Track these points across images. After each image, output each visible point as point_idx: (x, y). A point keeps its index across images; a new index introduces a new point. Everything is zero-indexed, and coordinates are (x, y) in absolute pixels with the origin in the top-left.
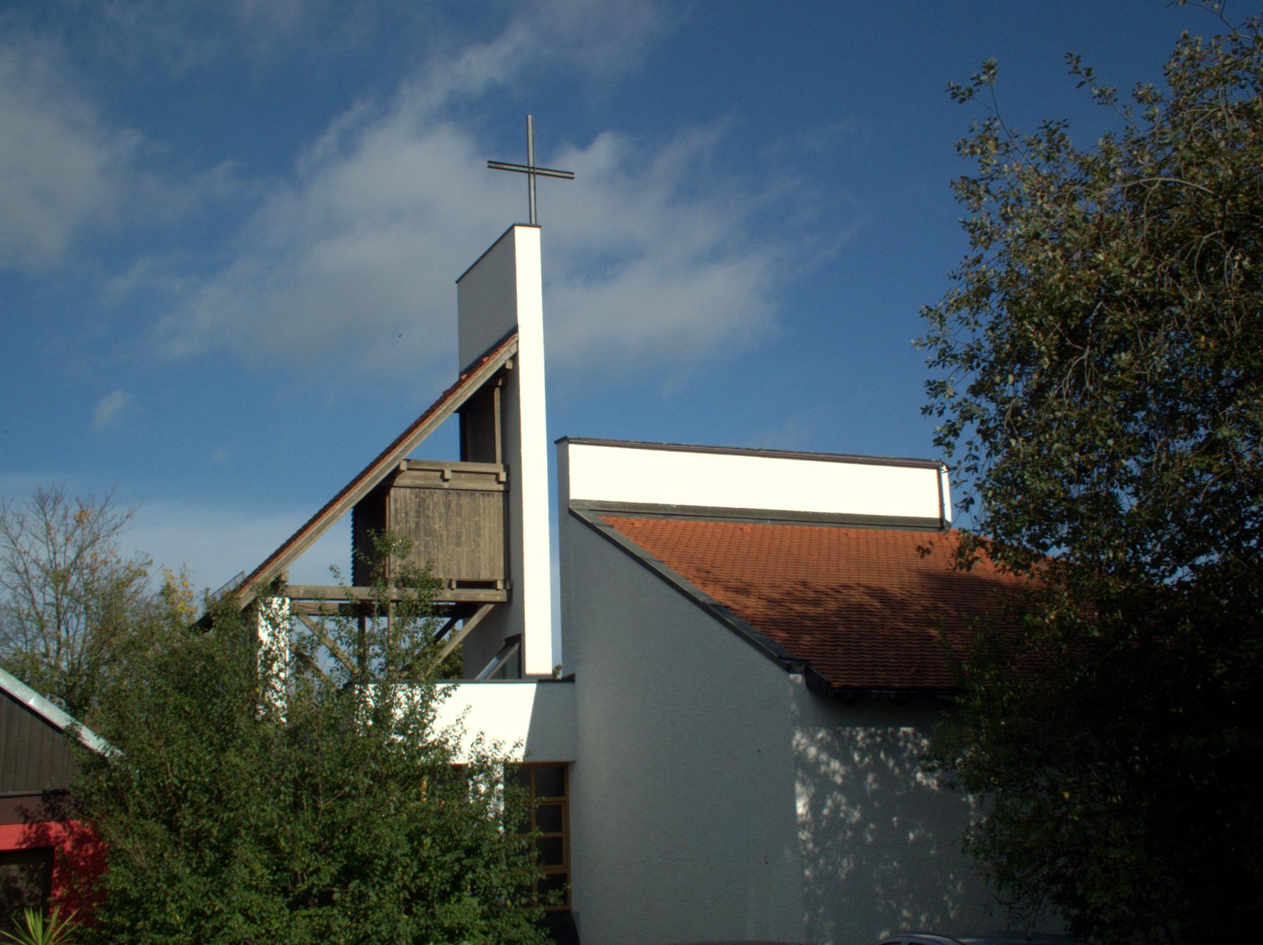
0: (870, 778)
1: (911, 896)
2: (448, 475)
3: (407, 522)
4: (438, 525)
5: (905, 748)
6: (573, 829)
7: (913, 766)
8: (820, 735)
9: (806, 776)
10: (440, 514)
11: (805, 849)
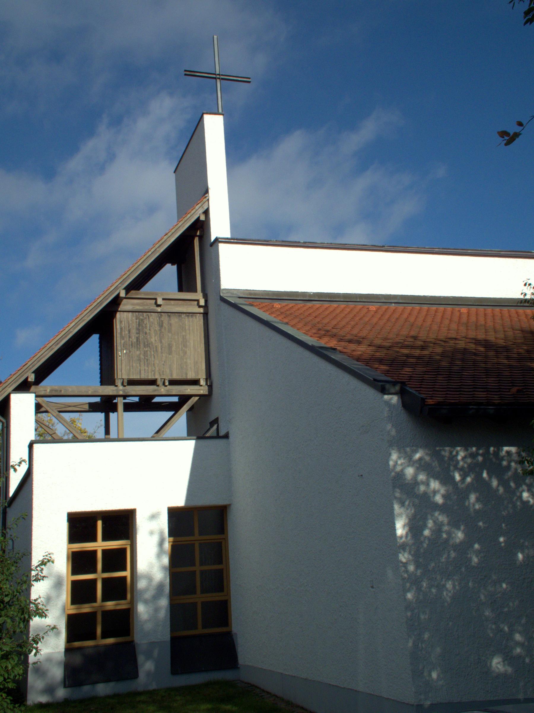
0: (473, 497)
1: (523, 621)
2: (160, 301)
3: (130, 337)
4: (154, 339)
5: (508, 467)
6: (231, 562)
7: (518, 486)
8: (417, 456)
9: (404, 497)
10: (155, 330)
11: (407, 571)
